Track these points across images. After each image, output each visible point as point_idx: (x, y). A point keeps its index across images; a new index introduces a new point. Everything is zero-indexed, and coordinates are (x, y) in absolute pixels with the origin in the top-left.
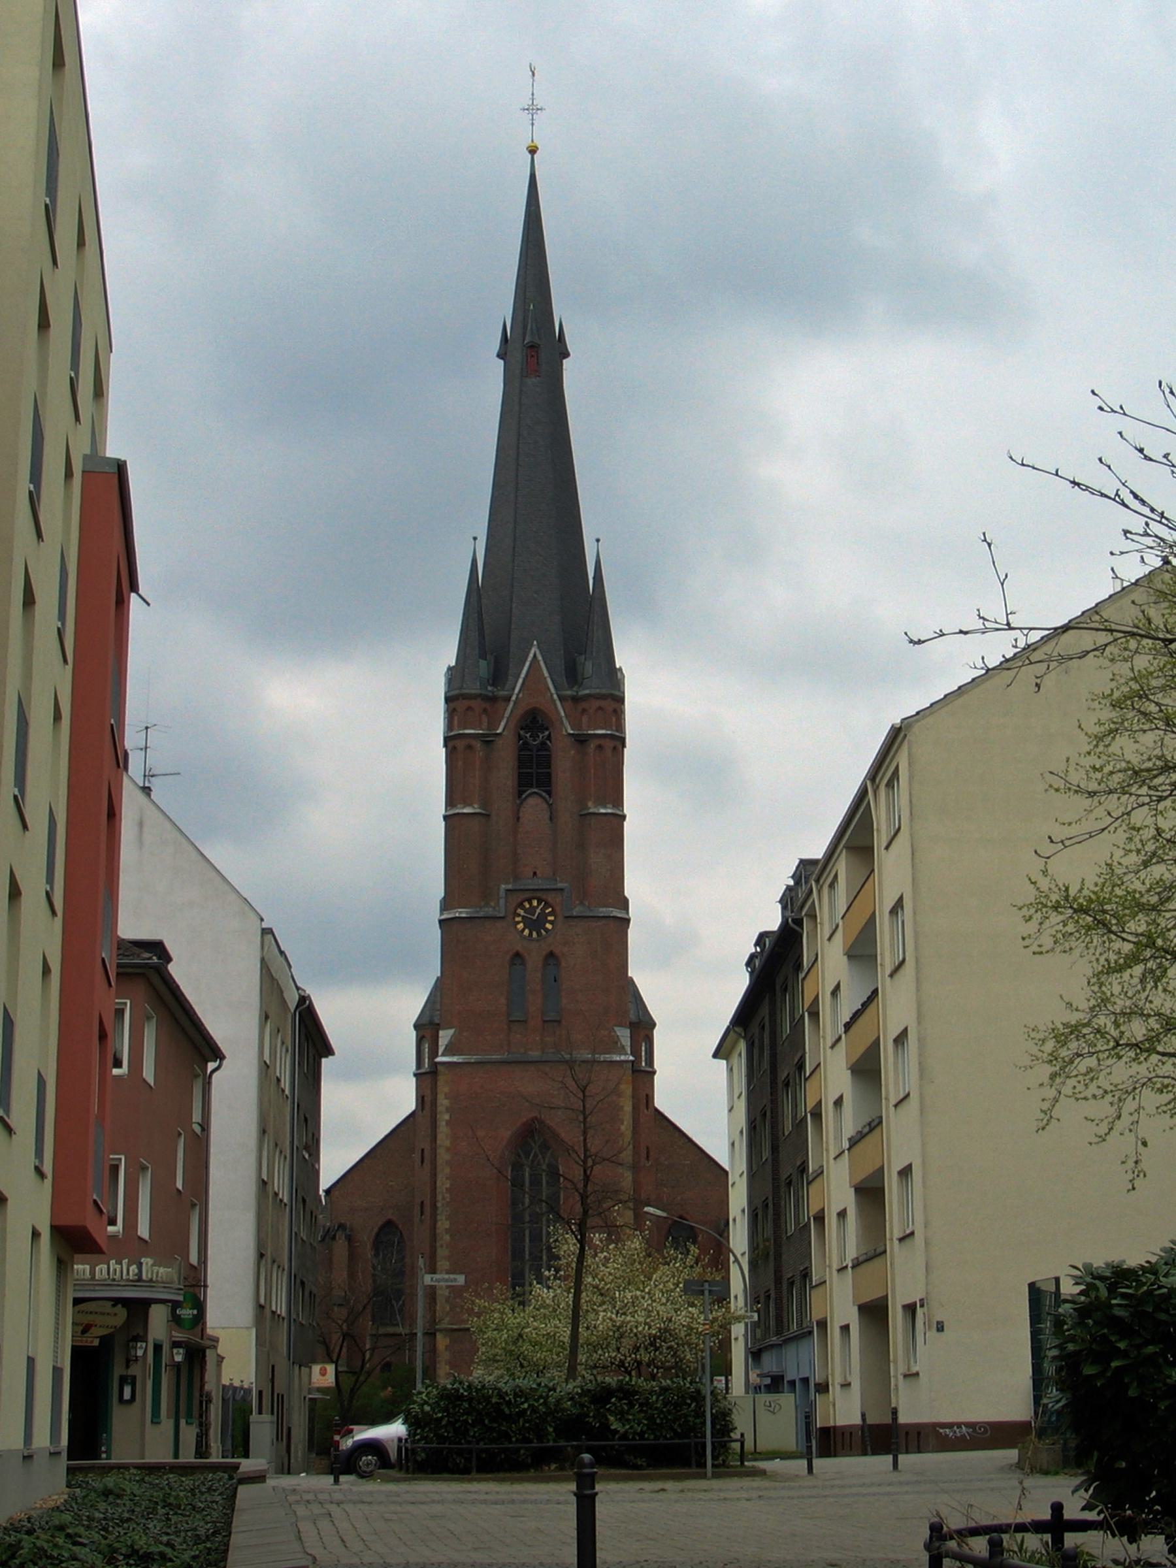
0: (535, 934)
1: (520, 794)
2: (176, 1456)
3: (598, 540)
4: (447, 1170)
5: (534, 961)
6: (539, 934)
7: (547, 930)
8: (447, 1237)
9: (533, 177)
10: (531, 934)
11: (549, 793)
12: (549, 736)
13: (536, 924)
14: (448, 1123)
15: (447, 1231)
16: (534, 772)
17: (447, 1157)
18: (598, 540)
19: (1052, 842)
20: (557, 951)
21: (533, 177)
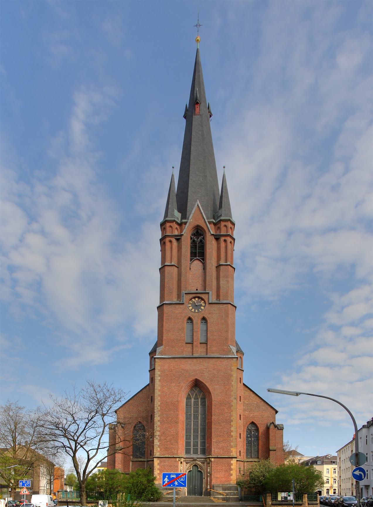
0: (197, 311)
1: (191, 260)
2: (193, 355)
3: (224, 167)
4: (159, 398)
5: (197, 320)
6: (198, 310)
7: (201, 309)
8: (159, 423)
9: (197, 64)
10: (195, 311)
11: (203, 259)
12: (203, 238)
13: (196, 306)
14: (160, 381)
15: (159, 421)
16: (198, 251)
17: (159, 393)
18: (224, 167)
19: (356, 206)
20: (206, 317)
21: (197, 64)
